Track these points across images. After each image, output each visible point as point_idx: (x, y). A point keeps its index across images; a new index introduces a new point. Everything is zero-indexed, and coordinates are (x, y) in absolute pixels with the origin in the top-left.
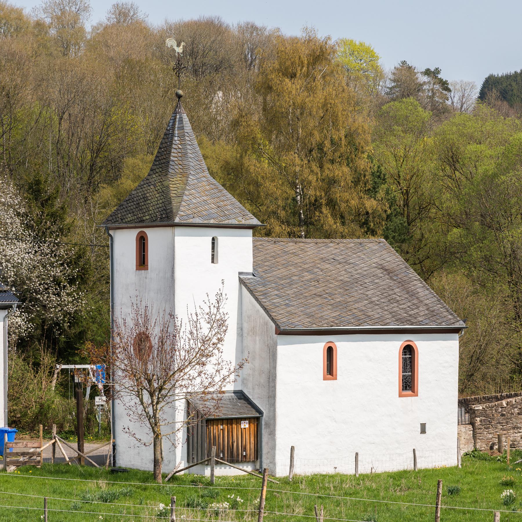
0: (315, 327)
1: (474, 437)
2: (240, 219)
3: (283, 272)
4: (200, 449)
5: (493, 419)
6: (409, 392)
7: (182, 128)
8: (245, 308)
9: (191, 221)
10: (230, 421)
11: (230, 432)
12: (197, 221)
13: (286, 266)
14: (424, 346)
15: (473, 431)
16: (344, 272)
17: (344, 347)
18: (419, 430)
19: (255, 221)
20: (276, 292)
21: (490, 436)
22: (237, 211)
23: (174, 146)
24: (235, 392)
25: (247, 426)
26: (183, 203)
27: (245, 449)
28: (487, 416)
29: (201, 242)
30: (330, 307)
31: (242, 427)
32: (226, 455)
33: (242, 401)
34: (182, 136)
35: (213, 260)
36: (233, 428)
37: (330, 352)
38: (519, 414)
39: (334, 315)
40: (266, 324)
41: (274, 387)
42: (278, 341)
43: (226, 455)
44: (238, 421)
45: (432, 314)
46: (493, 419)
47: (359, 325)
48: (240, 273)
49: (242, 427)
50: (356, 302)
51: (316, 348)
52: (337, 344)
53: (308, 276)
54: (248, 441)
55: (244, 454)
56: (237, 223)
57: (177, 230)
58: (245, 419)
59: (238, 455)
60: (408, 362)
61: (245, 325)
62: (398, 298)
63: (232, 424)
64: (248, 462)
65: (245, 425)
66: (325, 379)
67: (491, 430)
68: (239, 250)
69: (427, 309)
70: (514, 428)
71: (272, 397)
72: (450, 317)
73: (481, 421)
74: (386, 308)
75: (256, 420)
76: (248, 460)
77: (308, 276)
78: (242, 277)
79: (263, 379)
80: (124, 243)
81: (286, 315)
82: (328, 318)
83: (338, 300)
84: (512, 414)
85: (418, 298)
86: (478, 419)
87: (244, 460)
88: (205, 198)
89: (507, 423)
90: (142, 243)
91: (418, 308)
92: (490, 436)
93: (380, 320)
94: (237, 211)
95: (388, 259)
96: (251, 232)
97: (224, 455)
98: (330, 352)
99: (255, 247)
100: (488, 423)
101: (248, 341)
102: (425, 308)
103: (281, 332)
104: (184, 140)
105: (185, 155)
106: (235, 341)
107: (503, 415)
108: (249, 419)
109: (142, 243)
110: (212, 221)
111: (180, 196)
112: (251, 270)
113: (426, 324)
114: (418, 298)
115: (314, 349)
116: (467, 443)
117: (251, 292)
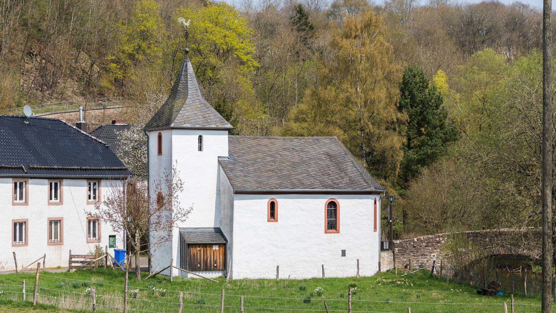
0: (260, 190)
1: (394, 260)
2: (218, 124)
3: (253, 156)
4: (189, 262)
5: (407, 249)
6: (334, 231)
7: (186, 71)
8: (221, 178)
9: (184, 126)
10: (205, 245)
11: (205, 253)
12: (188, 125)
13: (255, 153)
14: (343, 203)
15: (394, 256)
16: (297, 157)
17: (282, 202)
18: (341, 254)
19: (229, 126)
20: (241, 168)
21: (405, 260)
22: (217, 120)
23: (181, 82)
24: (215, 228)
25: (217, 248)
26: (179, 115)
27: (216, 262)
28: (403, 247)
29: (192, 138)
30: (276, 178)
31: (214, 249)
32: (202, 266)
33: (218, 234)
34: (186, 76)
35: (200, 149)
36: (208, 249)
37: (273, 206)
38: (426, 246)
39: (277, 182)
40: (229, 187)
41: (232, 225)
42: (235, 198)
43: (202, 266)
44: (211, 245)
45: (352, 182)
46: (407, 249)
47: (293, 189)
48: (219, 157)
49: (214, 249)
50: (297, 175)
51: (263, 203)
52: (278, 200)
53: (269, 159)
54: (218, 258)
55: (215, 265)
56: (215, 127)
57: (174, 131)
58: (216, 244)
59: (211, 266)
60: (333, 212)
61: (221, 188)
62: (331, 173)
63: (206, 247)
64: (219, 270)
65: (215, 248)
66: (268, 221)
67: (405, 256)
68: (218, 144)
69: (349, 180)
70: (422, 255)
71: (231, 231)
72: (365, 184)
73: (398, 250)
74: (318, 179)
75: (224, 245)
76: (218, 268)
77: (269, 159)
78: (220, 159)
79: (228, 221)
80: (153, 137)
81: (239, 181)
82: (273, 183)
83: (284, 173)
84: (421, 246)
85: (345, 173)
86: (397, 249)
87: (215, 269)
88: (195, 112)
89: (417, 252)
90: (160, 137)
91: (343, 178)
92: (405, 260)
93: (280, 185)
94: (217, 120)
95: (334, 149)
96: (227, 132)
97: (200, 265)
98: (273, 206)
99: (230, 142)
100: (403, 251)
101: (222, 196)
102: (348, 178)
103: (236, 193)
104: (187, 78)
105: (187, 87)
106: (215, 198)
107: (414, 247)
108: (219, 245)
109: (160, 137)
110: (197, 126)
111: (178, 111)
112: (227, 155)
113: (344, 189)
114: (345, 173)
115: (262, 204)
116: (390, 263)
117: (223, 168)
